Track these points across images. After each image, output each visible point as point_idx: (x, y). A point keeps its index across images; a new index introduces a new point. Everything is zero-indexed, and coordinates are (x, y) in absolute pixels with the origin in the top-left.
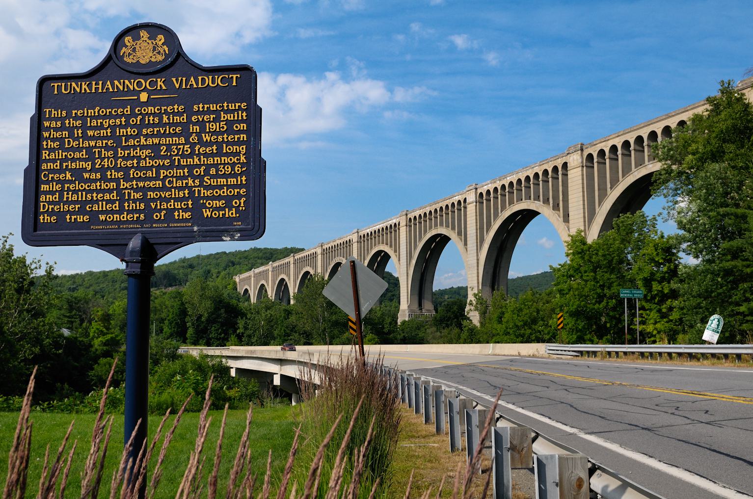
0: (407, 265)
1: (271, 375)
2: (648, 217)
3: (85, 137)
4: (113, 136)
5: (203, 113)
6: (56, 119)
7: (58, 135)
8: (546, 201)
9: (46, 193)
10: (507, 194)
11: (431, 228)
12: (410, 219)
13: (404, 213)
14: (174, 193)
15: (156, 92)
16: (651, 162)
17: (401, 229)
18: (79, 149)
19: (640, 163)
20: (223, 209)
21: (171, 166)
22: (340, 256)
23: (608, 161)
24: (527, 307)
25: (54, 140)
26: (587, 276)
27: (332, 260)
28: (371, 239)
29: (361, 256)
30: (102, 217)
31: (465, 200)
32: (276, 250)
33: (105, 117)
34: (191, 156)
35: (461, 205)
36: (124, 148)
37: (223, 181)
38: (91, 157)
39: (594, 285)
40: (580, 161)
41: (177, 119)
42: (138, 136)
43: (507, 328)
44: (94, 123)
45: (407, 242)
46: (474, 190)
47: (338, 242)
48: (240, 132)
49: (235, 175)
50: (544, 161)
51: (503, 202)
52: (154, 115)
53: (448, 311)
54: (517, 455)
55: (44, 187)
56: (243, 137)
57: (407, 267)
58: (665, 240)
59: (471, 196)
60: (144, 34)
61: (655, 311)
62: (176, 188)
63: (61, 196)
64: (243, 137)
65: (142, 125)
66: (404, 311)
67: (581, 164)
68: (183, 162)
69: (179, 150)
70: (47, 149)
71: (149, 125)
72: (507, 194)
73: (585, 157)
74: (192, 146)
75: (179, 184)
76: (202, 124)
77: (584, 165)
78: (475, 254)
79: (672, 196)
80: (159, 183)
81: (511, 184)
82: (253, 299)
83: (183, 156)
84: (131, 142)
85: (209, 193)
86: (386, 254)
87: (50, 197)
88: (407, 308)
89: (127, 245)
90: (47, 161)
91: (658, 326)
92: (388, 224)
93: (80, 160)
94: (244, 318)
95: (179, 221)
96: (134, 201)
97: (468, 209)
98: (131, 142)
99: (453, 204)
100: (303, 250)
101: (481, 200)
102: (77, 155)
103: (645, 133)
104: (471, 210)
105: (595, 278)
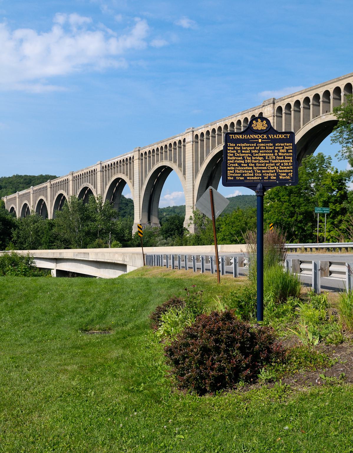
0: (139, 189)
1: (50, 270)
2: (325, 156)
3: (242, 153)
4: (251, 153)
5: (279, 146)
6: (232, 147)
7: (233, 152)
9: (230, 170)
10: (216, 136)
11: (158, 161)
12: (142, 154)
13: (137, 149)
14: (270, 171)
15: (264, 139)
16: (324, 114)
17: (134, 161)
18: (240, 157)
19: (316, 115)
20: (286, 176)
21: (269, 163)
22: (87, 182)
23: (293, 112)
24: (239, 220)
25: (231, 153)
26: (284, 198)
27: (81, 185)
28: (111, 169)
29: (103, 182)
30: (248, 178)
31: (184, 140)
32: (34, 177)
33: (248, 147)
34: (275, 160)
35: (182, 143)
36: (254, 157)
37: (285, 168)
38: (244, 159)
39: (289, 205)
40: (272, 112)
41: (271, 148)
42: (259, 153)
43: (224, 236)
44: (244, 148)
45: (139, 172)
46: (191, 132)
47: (86, 171)
48: (290, 153)
49: (289, 166)
50: (245, 111)
51: (214, 142)
52: (264, 146)
53: (172, 224)
54: (323, 272)
55: (229, 168)
56: (291, 154)
57: (139, 191)
58: (338, 174)
59: (189, 137)
60: (265, 122)
61: (330, 223)
62: (271, 169)
63: (235, 171)
64: (291, 154)
65: (260, 150)
67: (273, 115)
68: (273, 161)
69: (271, 158)
70: (229, 156)
71: (262, 150)
72: (216, 136)
74: (276, 157)
75: (272, 168)
76: (279, 150)
77: (275, 115)
78: (192, 182)
79: (346, 143)
80: (266, 168)
81: (220, 128)
82: (18, 214)
83: (273, 160)
84: (256, 155)
85: (281, 171)
86: (123, 180)
87: (231, 172)
89: (256, 186)
90: (229, 160)
91: (332, 233)
92: (124, 157)
93: (240, 160)
94: (17, 229)
95: (272, 180)
96: (258, 173)
97: (187, 147)
98: (256, 155)
99: (175, 143)
100: (54, 177)
101: (196, 140)
102: (239, 158)
103: (321, 92)
104: (189, 147)
105: (289, 200)
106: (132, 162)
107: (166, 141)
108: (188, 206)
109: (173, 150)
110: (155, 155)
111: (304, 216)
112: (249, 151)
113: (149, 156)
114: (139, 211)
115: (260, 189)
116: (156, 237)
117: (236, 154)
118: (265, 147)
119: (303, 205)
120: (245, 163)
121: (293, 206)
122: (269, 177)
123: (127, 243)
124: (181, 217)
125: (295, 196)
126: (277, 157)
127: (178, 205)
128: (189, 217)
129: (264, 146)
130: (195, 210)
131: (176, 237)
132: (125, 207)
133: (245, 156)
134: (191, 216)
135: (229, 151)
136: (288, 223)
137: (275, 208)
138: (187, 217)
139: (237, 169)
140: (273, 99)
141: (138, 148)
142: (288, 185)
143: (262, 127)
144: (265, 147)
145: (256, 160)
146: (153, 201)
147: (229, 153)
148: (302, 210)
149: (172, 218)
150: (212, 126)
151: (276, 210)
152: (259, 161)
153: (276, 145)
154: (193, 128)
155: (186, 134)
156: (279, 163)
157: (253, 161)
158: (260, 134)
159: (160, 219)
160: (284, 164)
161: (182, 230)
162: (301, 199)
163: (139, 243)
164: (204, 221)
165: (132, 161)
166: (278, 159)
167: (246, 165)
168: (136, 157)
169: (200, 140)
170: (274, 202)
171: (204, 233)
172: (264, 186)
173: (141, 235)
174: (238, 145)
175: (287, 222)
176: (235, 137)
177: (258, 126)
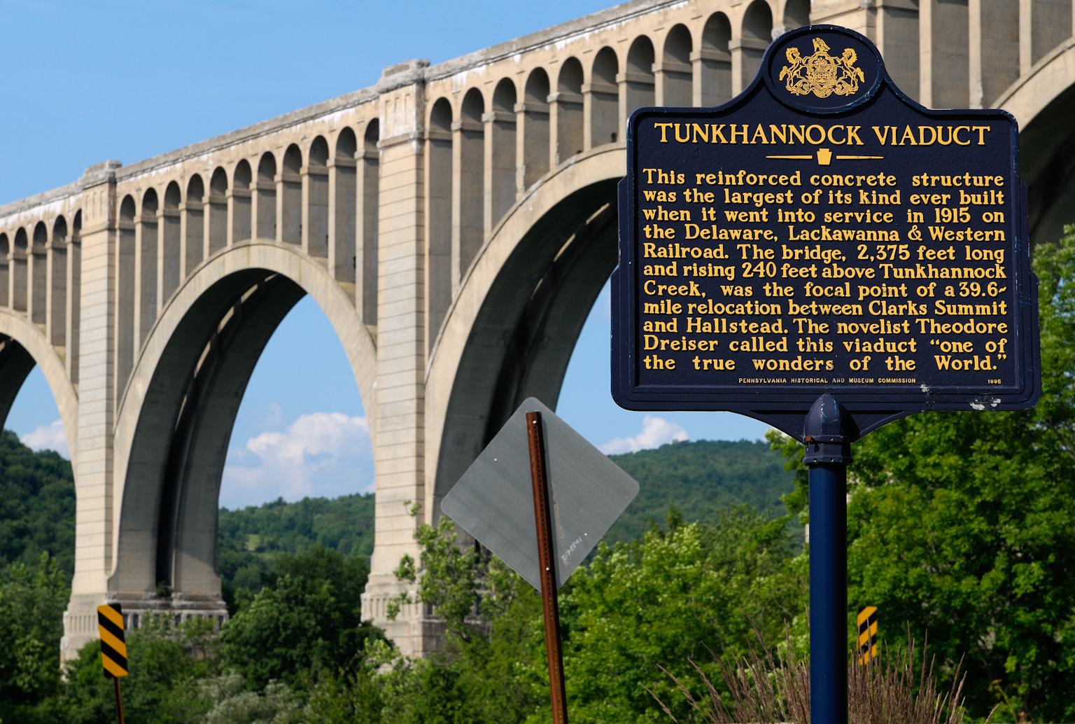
0: (109, 399)
3: (722, 223)
4: (772, 223)
5: (929, 190)
6: (667, 188)
7: (672, 215)
9: (654, 318)
10: (554, 110)
13: (102, 175)
14: (885, 327)
15: (845, 149)
17: (85, 242)
18: (713, 244)
20: (969, 356)
21: (878, 280)
25: (664, 225)
30: (759, 364)
31: (373, 129)
33: (756, 189)
34: (911, 263)
36: (793, 245)
37: (966, 309)
38: (734, 258)
39: (961, 505)
41: (884, 199)
42: (818, 223)
44: (737, 198)
45: (110, 303)
46: (413, 89)
48: (993, 226)
49: (988, 300)
51: (537, 144)
52: (845, 189)
56: (1000, 235)
57: (109, 411)
60: (850, 55)
62: (887, 318)
64: (1000, 235)
68: (898, 274)
70: (651, 240)
71: (835, 208)
72: (554, 110)
74: (913, 246)
75: (893, 310)
76: (928, 210)
78: (412, 362)
80: (857, 309)
83: (898, 263)
84: (805, 235)
85: (943, 329)
89: (806, 412)
90: (653, 262)
92: (28, 218)
93: (715, 262)
95: (894, 374)
97: (385, 169)
98: (805, 235)
101: (441, 132)
102: (709, 253)
105: (964, 476)
106: (70, 248)
107: (268, 132)
108: (392, 502)
109: (305, 181)
110: (207, 209)
111: (1051, 565)
112: (764, 213)
113: (173, 211)
114: (101, 527)
115: (826, 426)
116: (203, 675)
117: (693, 231)
118: (854, 191)
119: (1043, 502)
120: (739, 281)
121: (983, 508)
122: (878, 360)
123: (30, 710)
124: (346, 560)
125: (998, 453)
126: (920, 251)
127: (332, 491)
128: (395, 564)
129: (845, 189)
130: (428, 519)
131: (315, 680)
132: (24, 498)
133: (742, 241)
134: (407, 559)
135: (649, 214)
136: (957, 603)
137: (884, 521)
138: (384, 563)
139: (696, 314)
140: (112, 166)
141: (107, 169)
142: (981, 407)
143: (834, 82)
144: (854, 191)
145: (801, 262)
146: (189, 466)
147: (650, 222)
148: (1036, 529)
149: (296, 568)
150: (530, 56)
151: (892, 533)
152: (819, 272)
153: (916, 180)
154: (421, 65)
155: (383, 97)
156: (932, 286)
157: (784, 268)
158: (827, 120)
159: (226, 572)
160: (957, 290)
161: (352, 636)
162: (1033, 470)
163: (98, 710)
164: (479, 586)
165: (69, 238)
166: (925, 262)
167: (749, 291)
168: (96, 218)
169: (462, 130)
170: (880, 483)
171: (481, 658)
172: (849, 407)
173: (117, 671)
174: (699, 176)
175: (950, 598)
176: (683, 136)
177: (812, 79)
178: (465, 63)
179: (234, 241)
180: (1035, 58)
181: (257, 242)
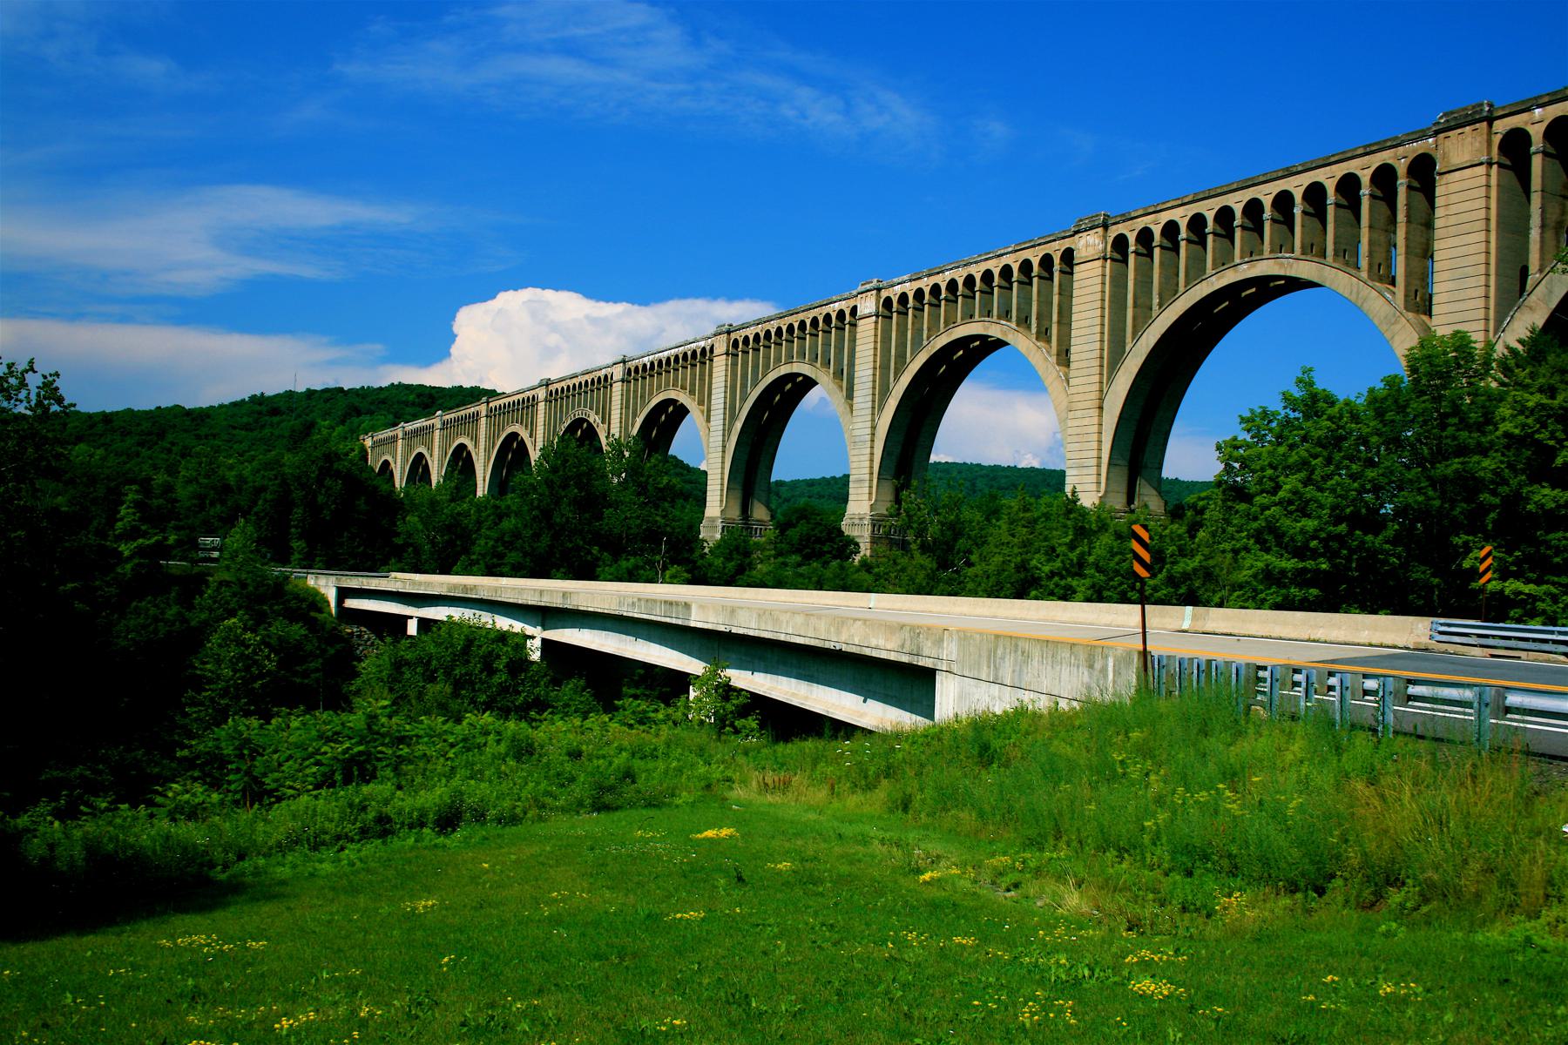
8: (1024, 321)
29: (627, 407)
31: (854, 310)
47: (582, 379)
51: (935, 319)
66: (713, 520)
73: (1497, 139)
78: (869, 418)
86: (590, 425)
88: (719, 514)
100: (492, 394)
107: (803, 311)
178: (900, 280)
179: (962, 319)
180: (1187, 283)
181: (1214, 272)
